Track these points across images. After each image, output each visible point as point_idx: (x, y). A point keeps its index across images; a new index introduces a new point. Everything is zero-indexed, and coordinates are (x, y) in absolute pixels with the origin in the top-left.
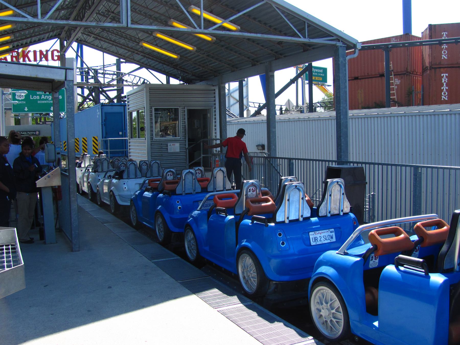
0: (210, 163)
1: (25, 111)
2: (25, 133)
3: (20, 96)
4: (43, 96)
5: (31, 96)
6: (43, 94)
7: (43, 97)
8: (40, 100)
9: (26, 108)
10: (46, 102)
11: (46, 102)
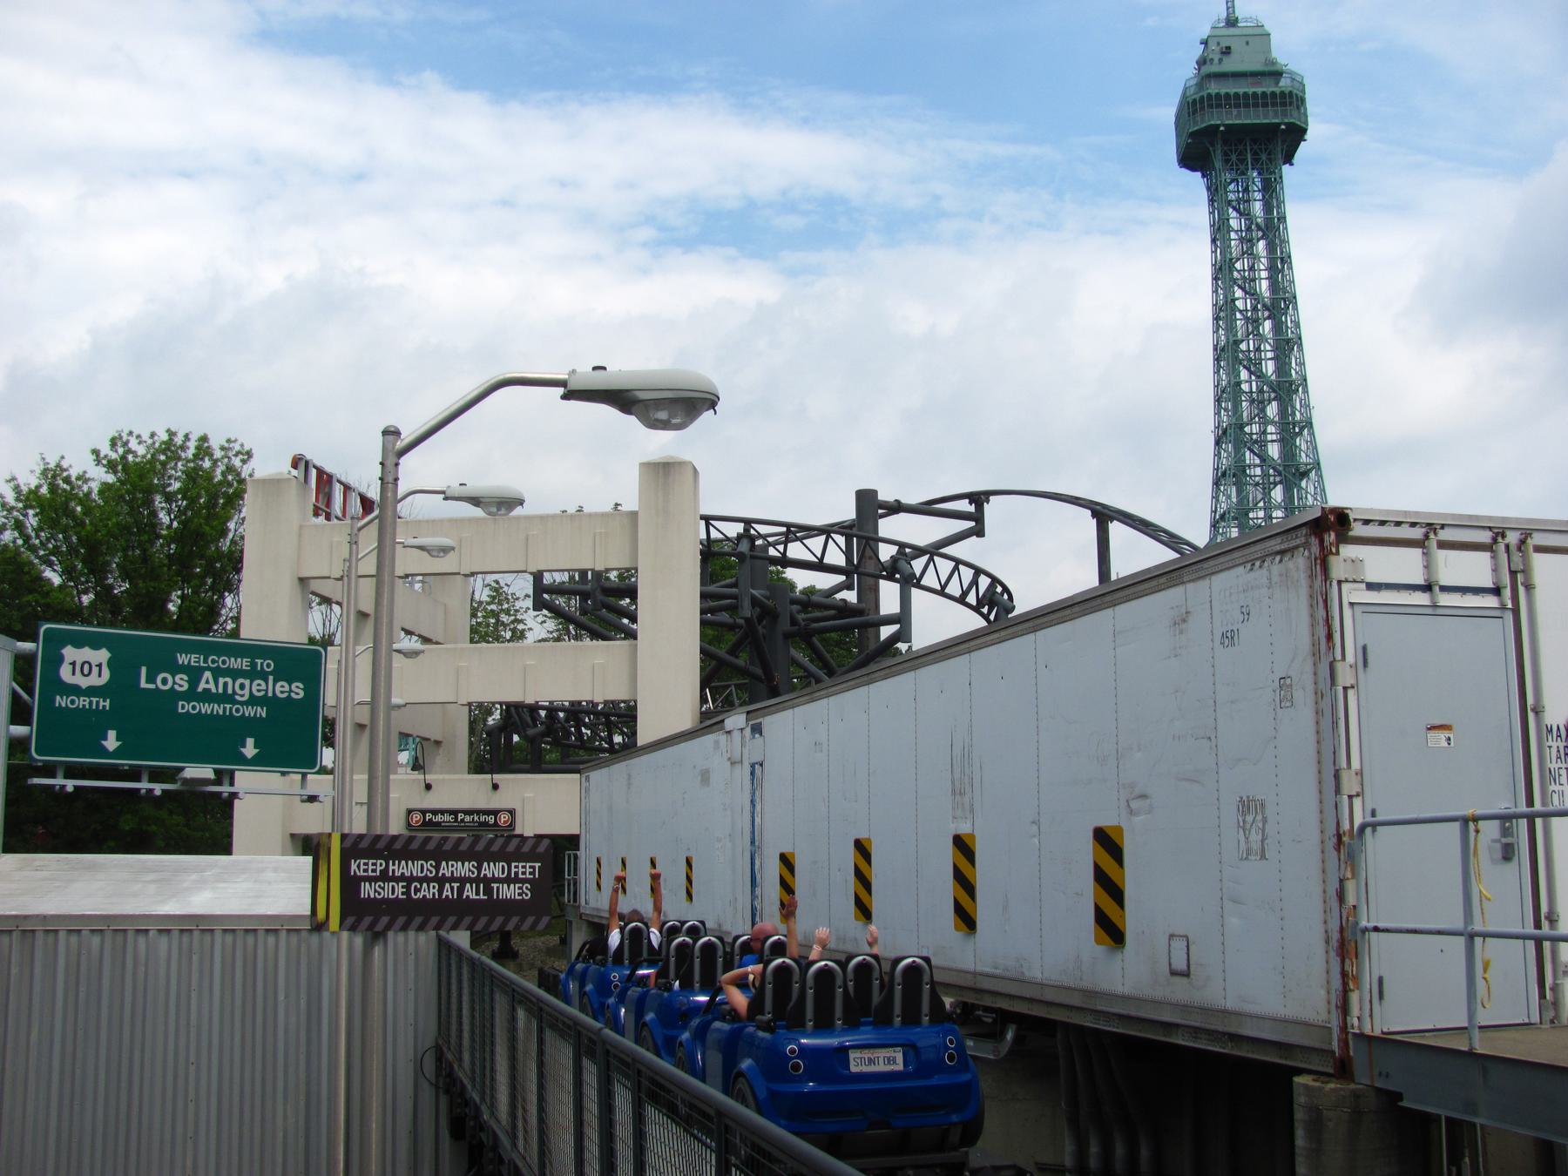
0: (1505, 810)
1: (104, 753)
2: (447, 818)
3: (86, 667)
4: (208, 674)
5: (144, 670)
6: (208, 668)
7: (207, 683)
8: (192, 695)
9: (112, 734)
10: (218, 709)
11: (218, 709)
